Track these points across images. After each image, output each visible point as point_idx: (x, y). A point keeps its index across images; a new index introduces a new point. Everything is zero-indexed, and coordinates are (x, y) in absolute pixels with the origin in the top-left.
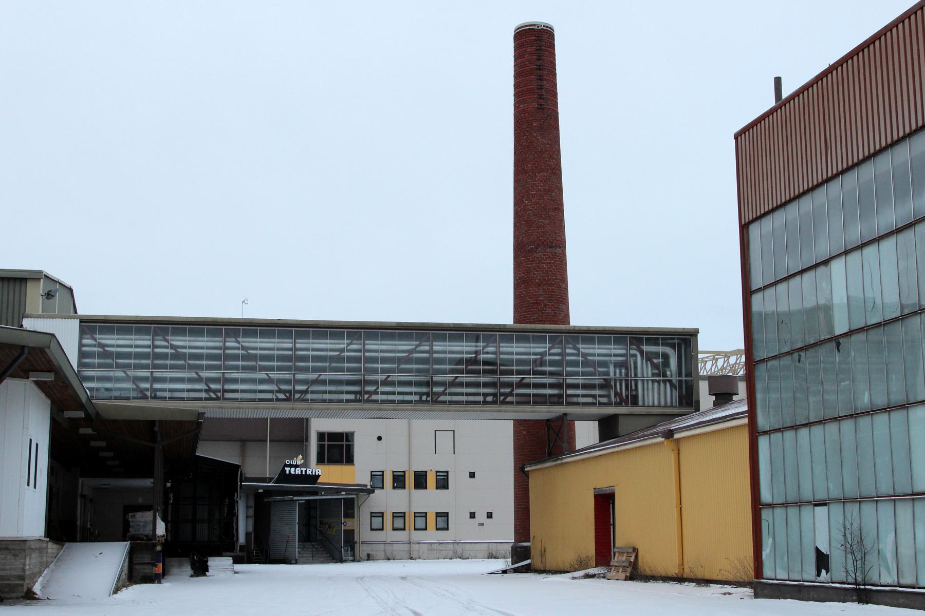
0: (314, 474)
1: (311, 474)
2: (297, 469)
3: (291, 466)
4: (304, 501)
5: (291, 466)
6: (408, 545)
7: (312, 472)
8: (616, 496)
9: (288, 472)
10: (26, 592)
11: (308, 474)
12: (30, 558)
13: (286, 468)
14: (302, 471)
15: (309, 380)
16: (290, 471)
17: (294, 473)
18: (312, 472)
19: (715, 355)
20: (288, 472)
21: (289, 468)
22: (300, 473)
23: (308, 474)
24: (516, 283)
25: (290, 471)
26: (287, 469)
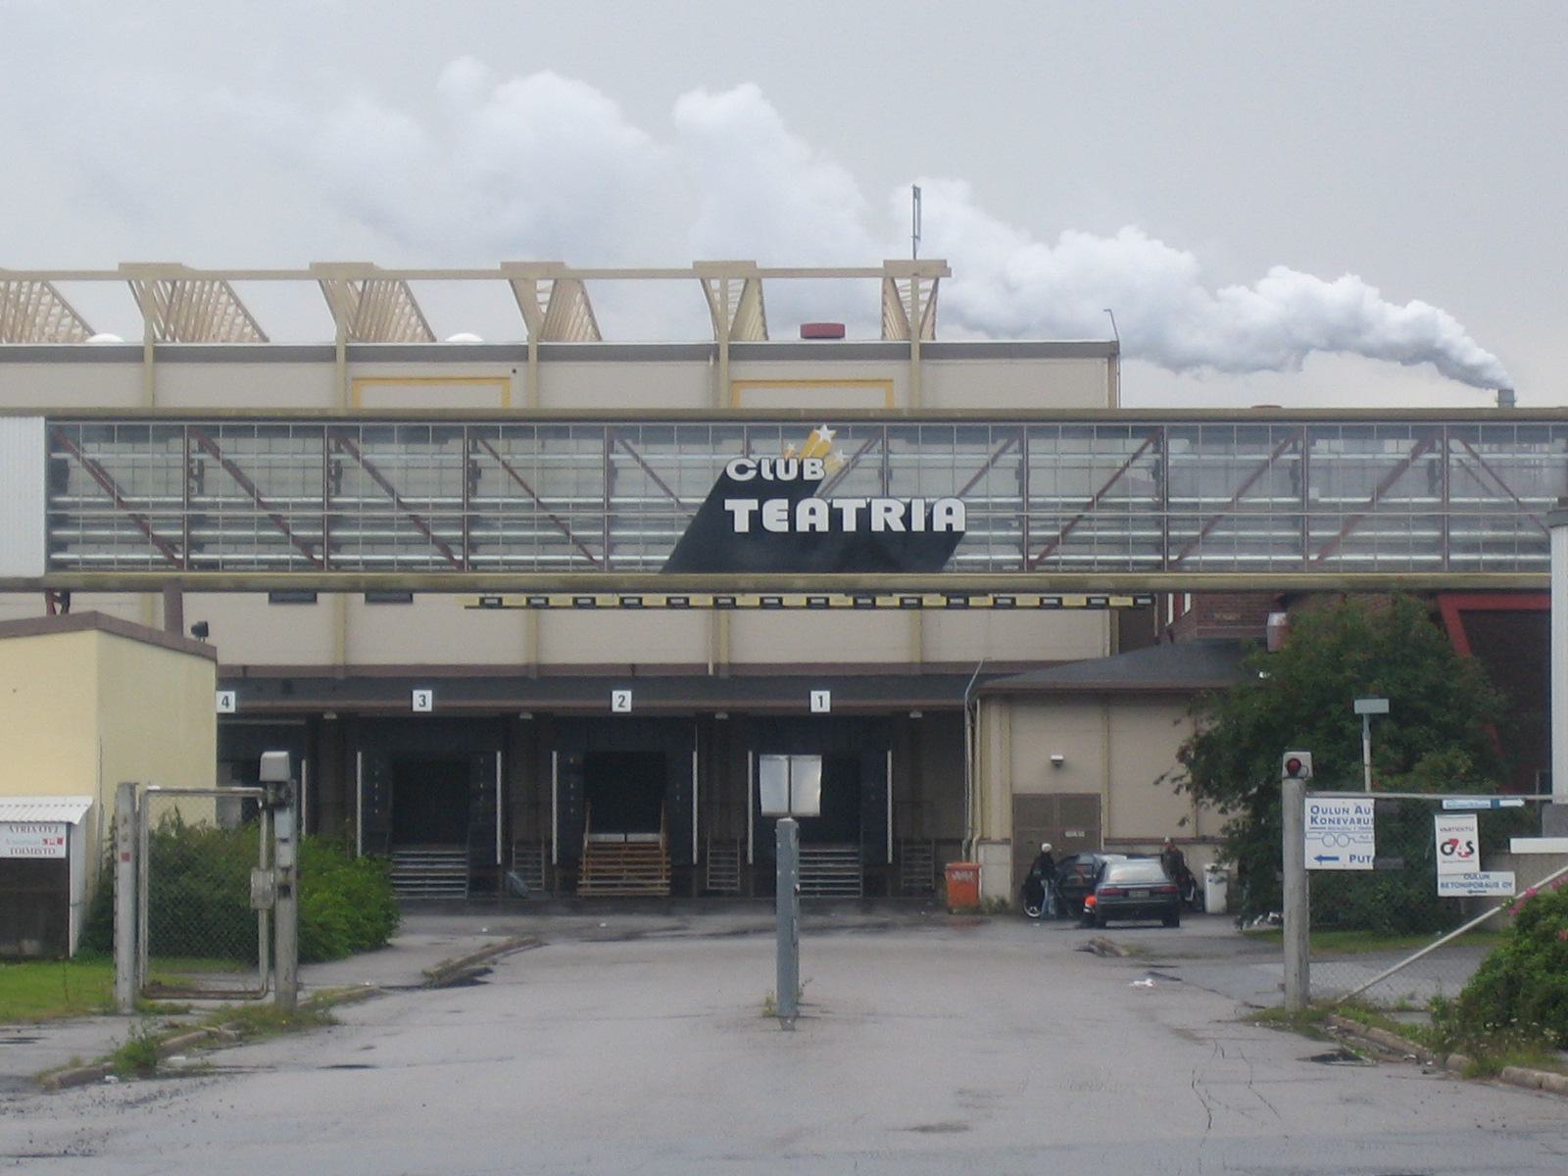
0: (918, 525)
1: (771, 477)
2: (803, 507)
3: (762, 489)
4: (1108, 924)
5: (762, 489)
6: (956, 471)
7: (907, 519)
8: (1374, 711)
9: (742, 525)
10: (453, 967)
11: (877, 526)
12: (101, 868)
13: (730, 504)
14: (836, 516)
15: (1098, 437)
16: (756, 517)
17: (784, 527)
18: (907, 519)
19: (301, 1001)
20: (742, 525)
21: (754, 504)
22: (823, 526)
23: (877, 526)
24: (1432, 838)
25: (756, 517)
26: (741, 510)
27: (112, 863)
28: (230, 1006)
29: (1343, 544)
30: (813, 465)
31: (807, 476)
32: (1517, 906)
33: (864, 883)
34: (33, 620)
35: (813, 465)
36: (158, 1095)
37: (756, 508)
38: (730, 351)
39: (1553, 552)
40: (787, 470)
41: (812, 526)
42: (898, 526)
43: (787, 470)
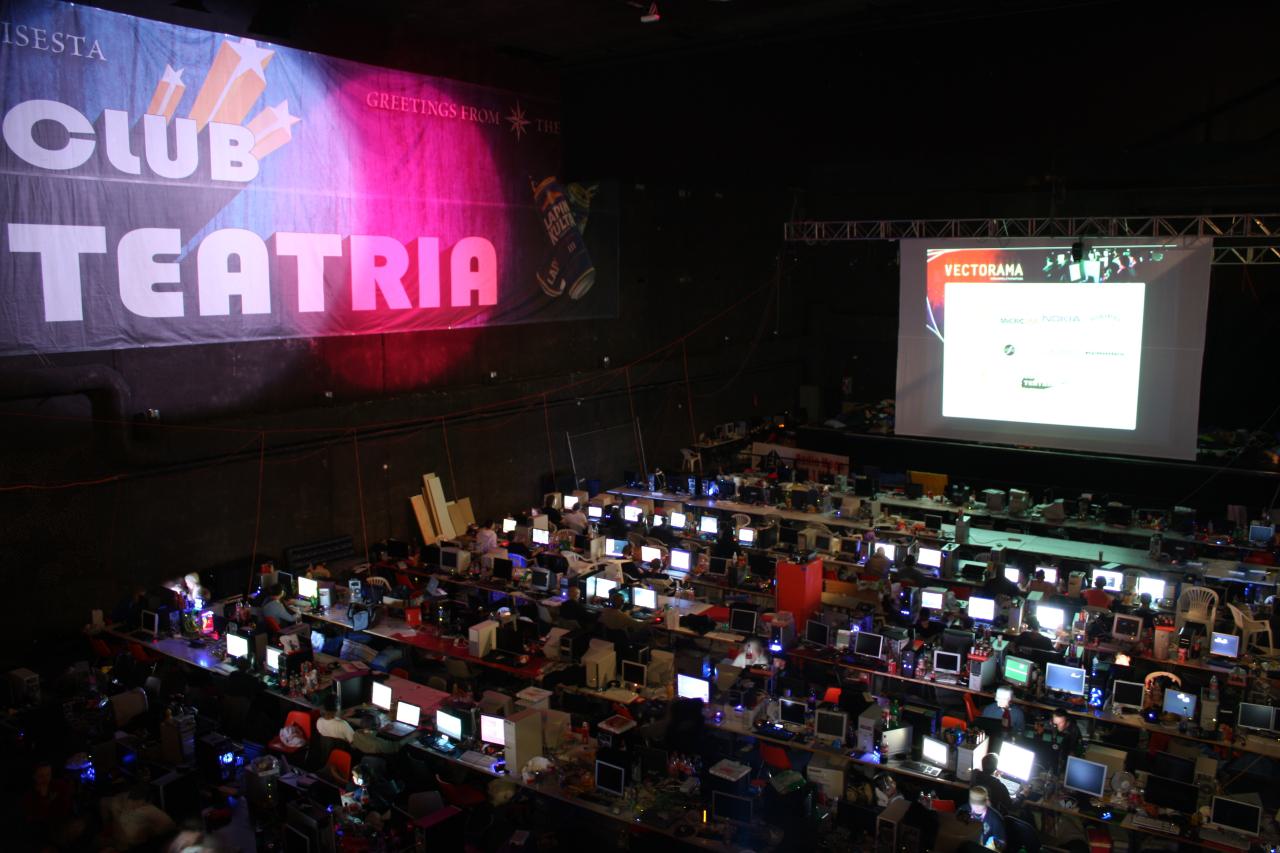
0: (430, 298)
16: (99, 273)
21: (93, 238)
25: (99, 273)
27: (568, 528)
28: (777, 456)
29: (436, 534)
30: (234, 143)
31: (221, 171)
32: (1036, 666)
33: (885, 219)
34: (443, 485)
35: (234, 143)
36: (1087, 278)
37: (100, 248)
38: (237, 55)
39: (446, 509)
40: (172, 154)
41: (235, 301)
42: (398, 300)
43: (172, 154)
